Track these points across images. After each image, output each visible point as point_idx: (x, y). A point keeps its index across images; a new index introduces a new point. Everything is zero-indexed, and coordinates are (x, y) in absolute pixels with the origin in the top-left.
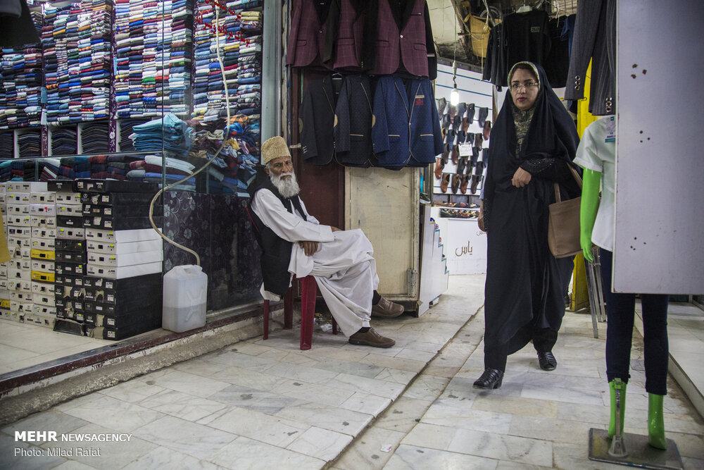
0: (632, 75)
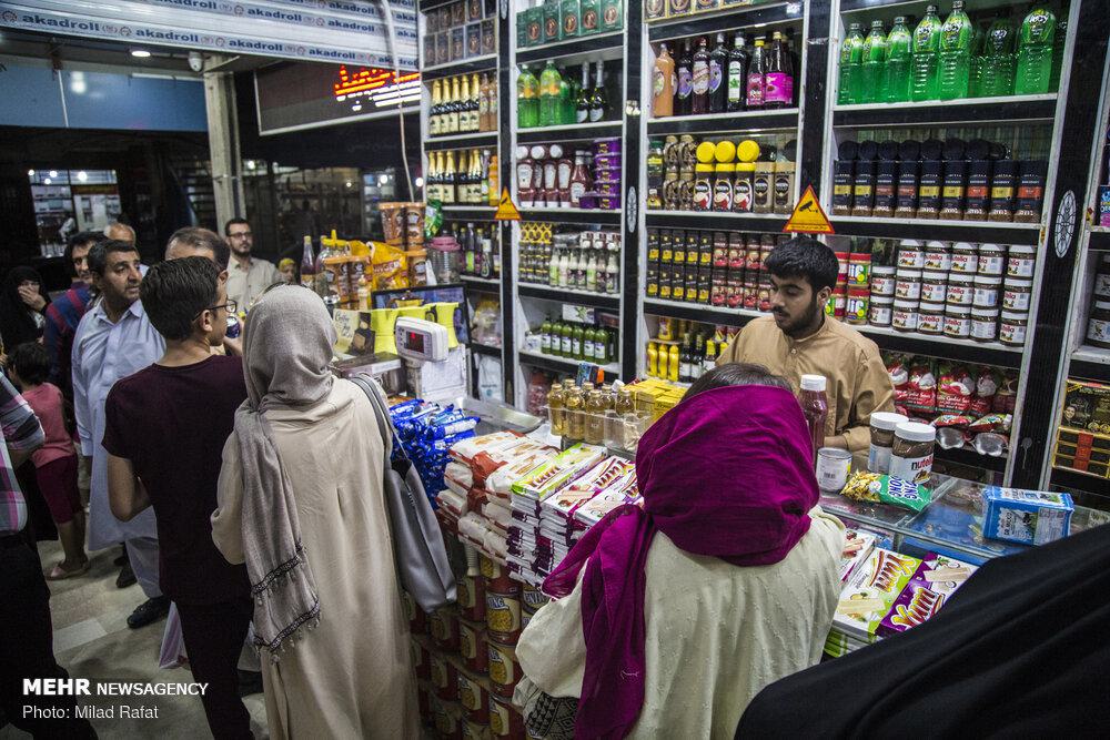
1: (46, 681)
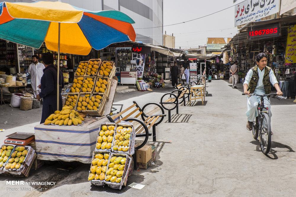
0: (59, 139)
1: (12, 181)
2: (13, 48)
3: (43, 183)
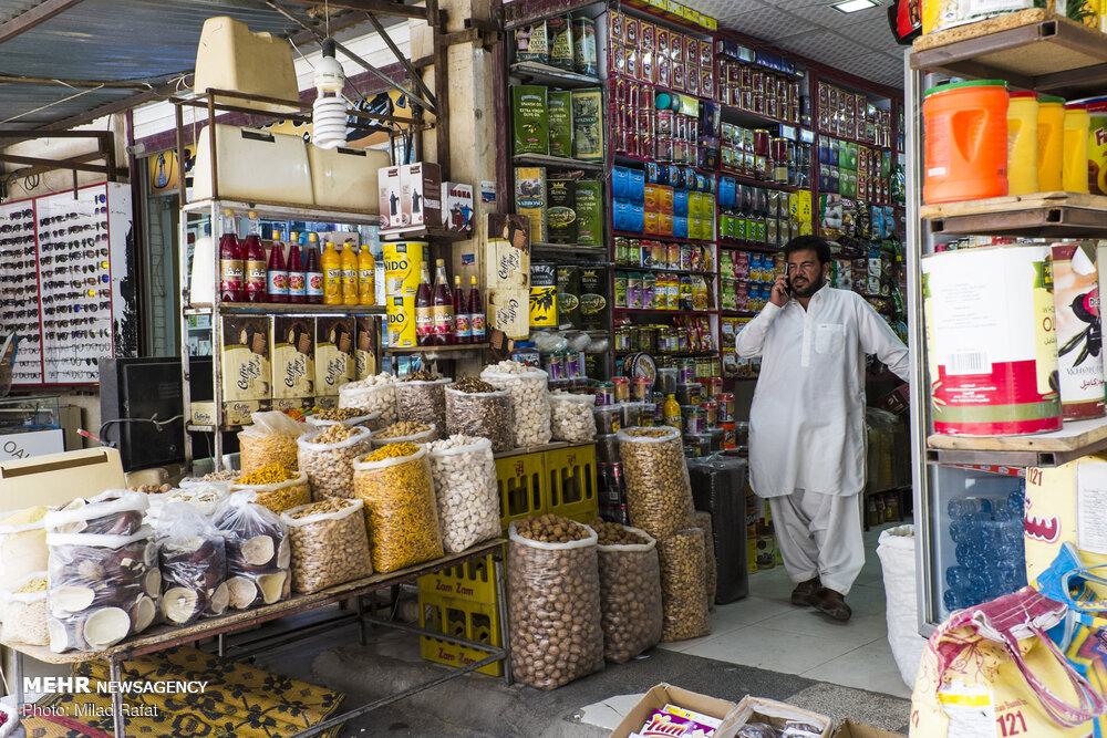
1: (46, 679)
2: (303, 283)
3: (160, 685)
